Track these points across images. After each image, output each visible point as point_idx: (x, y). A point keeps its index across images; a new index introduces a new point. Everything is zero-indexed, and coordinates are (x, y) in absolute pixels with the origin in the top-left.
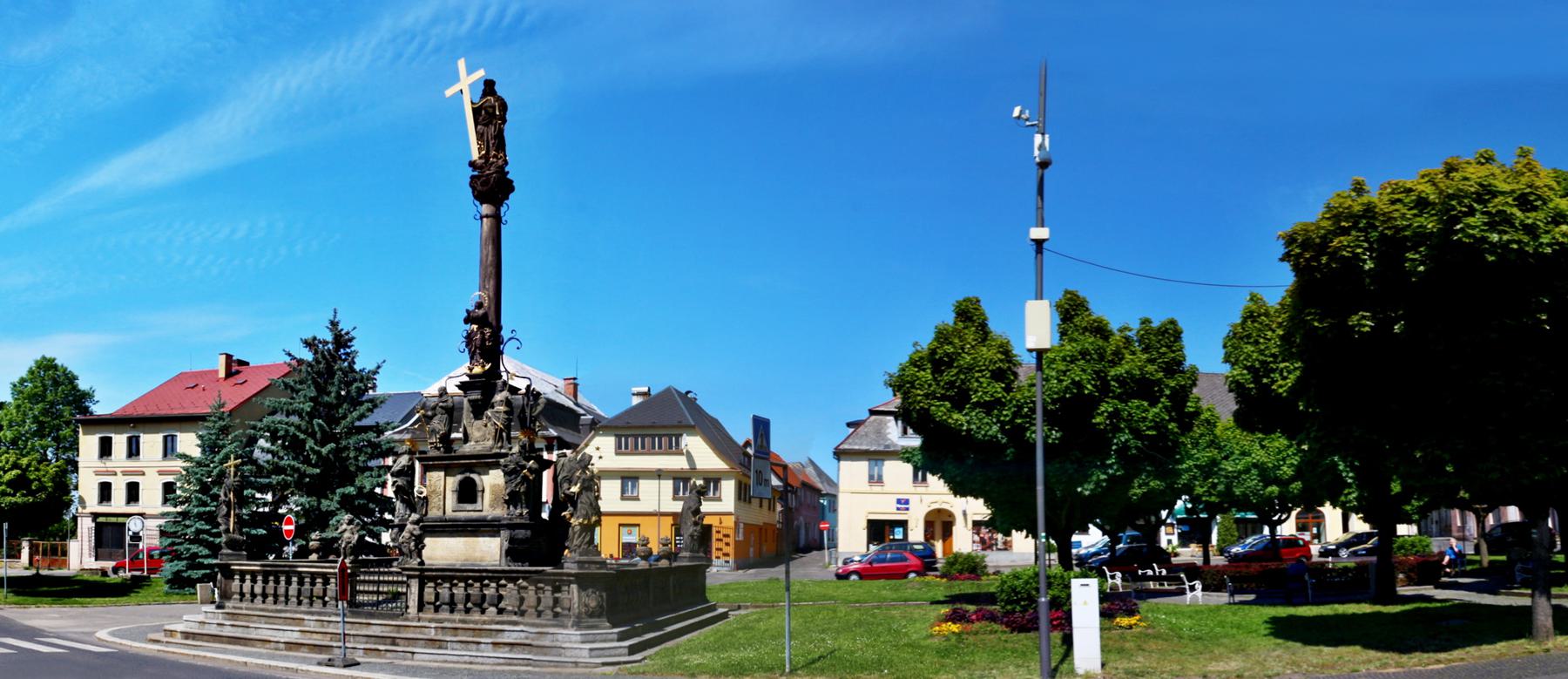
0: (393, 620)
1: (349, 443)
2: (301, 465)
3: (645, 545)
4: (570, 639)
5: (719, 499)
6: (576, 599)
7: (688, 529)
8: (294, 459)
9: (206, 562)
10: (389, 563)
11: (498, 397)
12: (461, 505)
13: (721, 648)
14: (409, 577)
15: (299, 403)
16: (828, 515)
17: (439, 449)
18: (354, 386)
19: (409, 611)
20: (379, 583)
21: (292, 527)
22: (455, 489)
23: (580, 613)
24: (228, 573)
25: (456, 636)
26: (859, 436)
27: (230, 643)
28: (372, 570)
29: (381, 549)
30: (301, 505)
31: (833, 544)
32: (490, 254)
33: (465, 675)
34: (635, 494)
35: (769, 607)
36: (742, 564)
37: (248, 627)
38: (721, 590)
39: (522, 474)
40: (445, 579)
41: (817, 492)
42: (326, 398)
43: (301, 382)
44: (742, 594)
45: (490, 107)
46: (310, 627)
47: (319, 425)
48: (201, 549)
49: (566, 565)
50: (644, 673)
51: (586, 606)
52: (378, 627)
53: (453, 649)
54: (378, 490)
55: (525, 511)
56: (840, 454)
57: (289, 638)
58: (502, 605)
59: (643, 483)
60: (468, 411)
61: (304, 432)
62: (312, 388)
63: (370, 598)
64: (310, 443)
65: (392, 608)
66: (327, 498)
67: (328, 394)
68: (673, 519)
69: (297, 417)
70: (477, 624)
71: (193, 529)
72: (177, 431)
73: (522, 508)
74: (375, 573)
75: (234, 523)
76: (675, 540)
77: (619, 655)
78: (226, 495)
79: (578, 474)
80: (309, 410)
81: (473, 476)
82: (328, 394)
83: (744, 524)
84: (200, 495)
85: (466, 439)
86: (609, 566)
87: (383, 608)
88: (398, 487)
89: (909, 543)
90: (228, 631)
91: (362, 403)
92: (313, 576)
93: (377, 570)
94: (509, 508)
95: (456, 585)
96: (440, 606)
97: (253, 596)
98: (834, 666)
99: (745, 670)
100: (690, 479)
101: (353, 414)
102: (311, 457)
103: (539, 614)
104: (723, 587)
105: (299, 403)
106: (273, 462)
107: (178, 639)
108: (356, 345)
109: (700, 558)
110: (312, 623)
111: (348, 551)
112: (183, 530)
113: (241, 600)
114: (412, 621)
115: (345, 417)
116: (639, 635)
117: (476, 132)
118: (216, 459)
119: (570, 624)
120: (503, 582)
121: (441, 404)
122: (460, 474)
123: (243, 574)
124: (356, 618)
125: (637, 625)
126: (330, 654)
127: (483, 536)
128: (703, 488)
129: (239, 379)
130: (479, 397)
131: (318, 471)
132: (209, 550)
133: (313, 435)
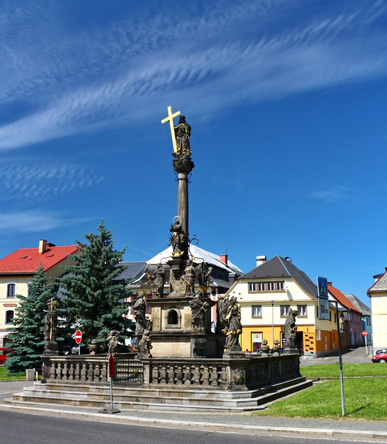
0: (136, 388)
1: (108, 290)
2: (83, 302)
3: (266, 344)
4: (226, 395)
5: (306, 317)
6: (229, 375)
7: (288, 335)
8: (79, 299)
9: (32, 356)
10: (132, 356)
11: (188, 269)
12: (170, 325)
13: (308, 402)
14: (144, 364)
15: (83, 268)
16: (367, 327)
17: (158, 295)
18: (112, 260)
19: (144, 382)
20: (128, 367)
21: (80, 337)
22: (166, 316)
23: (231, 382)
24: (49, 363)
25: (169, 396)
26: (381, 283)
27: (49, 402)
28: (125, 360)
29: (126, 349)
30: (83, 324)
31: (370, 344)
32: (183, 197)
33: (176, 417)
34: (260, 315)
35: (336, 379)
36: (321, 354)
37: (59, 393)
38: (309, 369)
39: (201, 309)
40: (163, 365)
41: (360, 314)
42: (96, 266)
43: (84, 257)
44: (320, 371)
45: (183, 128)
46: (93, 392)
47: (94, 280)
48: (28, 349)
49: (224, 356)
50: (266, 415)
51: (235, 378)
52: (129, 392)
53: (168, 403)
54: (123, 316)
55: (203, 329)
56: (370, 294)
57: (81, 398)
58: (193, 379)
59: (263, 309)
60: (172, 275)
61: (85, 284)
62: (90, 260)
63: (124, 376)
64: (88, 290)
65: (136, 381)
66: (96, 320)
67: (98, 263)
68: (281, 329)
69: (81, 276)
70: (180, 389)
71: (25, 338)
72: (16, 282)
73: (201, 326)
74: (126, 362)
75: (52, 335)
76: (283, 341)
77: (253, 406)
78: (48, 320)
79: (230, 307)
80: (88, 272)
81: (176, 309)
82: (98, 263)
83: (321, 331)
84: (29, 319)
85: (172, 290)
86: (246, 356)
87: (131, 381)
88: (137, 315)
89: (226, 366)
90: (48, 396)
91: (115, 269)
92: (94, 364)
93: (127, 360)
94: (194, 327)
95: (169, 368)
96: (161, 380)
97: (62, 375)
98: (369, 412)
99: (321, 414)
100: (289, 306)
101: (111, 274)
102: (89, 297)
103: (210, 383)
104: (310, 368)
105: (83, 268)
106: (69, 300)
107: (21, 401)
108: (113, 239)
109: (295, 351)
110: (94, 390)
111: (113, 350)
112: (18, 338)
113: (55, 378)
114: (146, 388)
115: (106, 276)
116: (263, 395)
117: (176, 140)
118: (38, 298)
119: (226, 388)
120: (193, 366)
121: (159, 272)
122: (169, 308)
123: (56, 363)
124: (117, 387)
125: (262, 389)
126: (103, 407)
127: (182, 342)
128: (296, 312)
129: (49, 254)
130: (178, 268)
131: (92, 305)
132: (33, 350)
133: (90, 285)
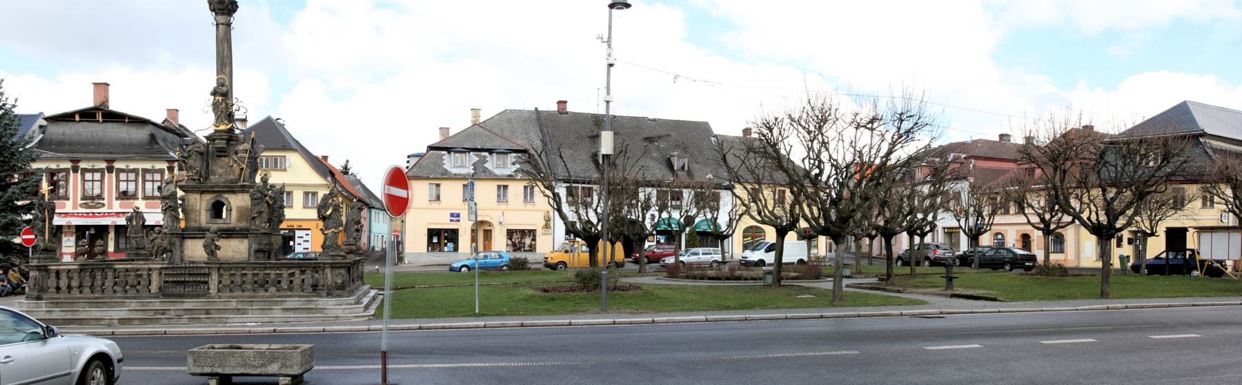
19: (210, 291)
97: (69, 288)
113: (58, 292)
114: (213, 298)
119: (325, 294)
121: (195, 149)
